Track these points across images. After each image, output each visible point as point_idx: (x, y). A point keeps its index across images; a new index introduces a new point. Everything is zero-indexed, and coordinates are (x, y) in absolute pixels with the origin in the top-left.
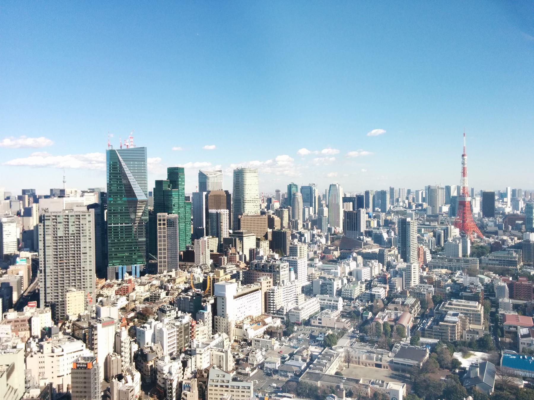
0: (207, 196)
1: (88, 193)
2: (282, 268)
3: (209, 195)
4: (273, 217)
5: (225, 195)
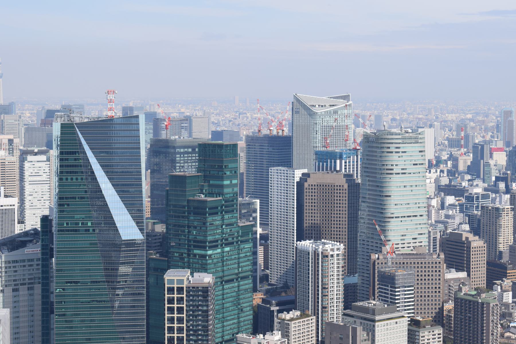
0: (300, 185)
1: (36, 154)
3: (306, 185)
4: (467, 238)
5: (346, 186)
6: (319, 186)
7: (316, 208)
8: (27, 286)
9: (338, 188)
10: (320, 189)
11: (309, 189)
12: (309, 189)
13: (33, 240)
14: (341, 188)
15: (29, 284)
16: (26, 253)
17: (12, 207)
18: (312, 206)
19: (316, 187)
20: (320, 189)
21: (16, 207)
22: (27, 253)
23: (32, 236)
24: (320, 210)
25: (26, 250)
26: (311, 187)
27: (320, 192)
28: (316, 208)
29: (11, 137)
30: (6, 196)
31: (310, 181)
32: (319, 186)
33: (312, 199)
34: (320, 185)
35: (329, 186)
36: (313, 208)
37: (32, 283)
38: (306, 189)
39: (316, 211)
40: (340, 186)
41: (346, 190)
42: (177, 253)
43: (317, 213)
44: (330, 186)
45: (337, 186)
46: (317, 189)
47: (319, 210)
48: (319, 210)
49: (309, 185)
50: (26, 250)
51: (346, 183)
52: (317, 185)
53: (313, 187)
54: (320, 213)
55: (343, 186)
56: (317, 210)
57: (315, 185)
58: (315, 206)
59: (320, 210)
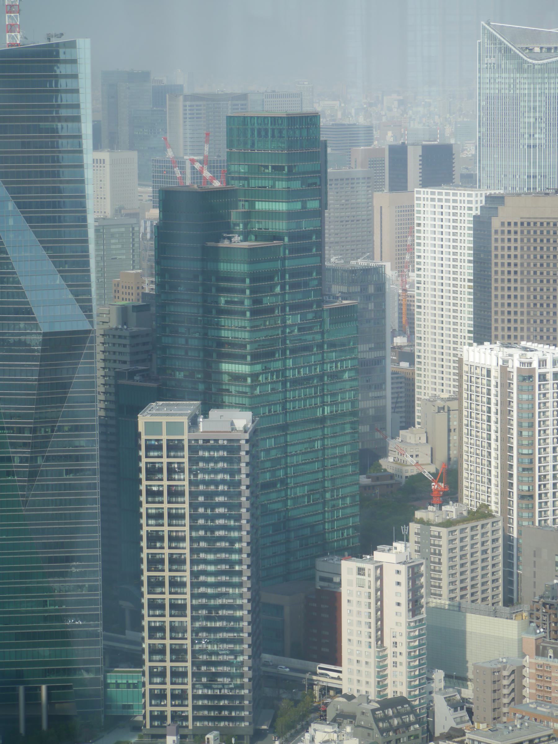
2: (361, 571)
6: (525, 224)
7: (519, 277)
10: (529, 232)
11: (503, 232)
18: (509, 264)
19: (519, 228)
20: (529, 232)
24: (529, 281)
26: (506, 229)
27: (529, 240)
28: (519, 277)
32: (525, 224)
33: (509, 232)
34: (529, 224)
36: (512, 277)
38: (496, 232)
39: (519, 285)
43: (522, 289)
46: (522, 232)
47: (525, 281)
48: (525, 281)
49: (503, 224)
52: (522, 224)
53: (512, 229)
54: (529, 289)
56: (522, 281)
57: (516, 224)
59: (529, 281)
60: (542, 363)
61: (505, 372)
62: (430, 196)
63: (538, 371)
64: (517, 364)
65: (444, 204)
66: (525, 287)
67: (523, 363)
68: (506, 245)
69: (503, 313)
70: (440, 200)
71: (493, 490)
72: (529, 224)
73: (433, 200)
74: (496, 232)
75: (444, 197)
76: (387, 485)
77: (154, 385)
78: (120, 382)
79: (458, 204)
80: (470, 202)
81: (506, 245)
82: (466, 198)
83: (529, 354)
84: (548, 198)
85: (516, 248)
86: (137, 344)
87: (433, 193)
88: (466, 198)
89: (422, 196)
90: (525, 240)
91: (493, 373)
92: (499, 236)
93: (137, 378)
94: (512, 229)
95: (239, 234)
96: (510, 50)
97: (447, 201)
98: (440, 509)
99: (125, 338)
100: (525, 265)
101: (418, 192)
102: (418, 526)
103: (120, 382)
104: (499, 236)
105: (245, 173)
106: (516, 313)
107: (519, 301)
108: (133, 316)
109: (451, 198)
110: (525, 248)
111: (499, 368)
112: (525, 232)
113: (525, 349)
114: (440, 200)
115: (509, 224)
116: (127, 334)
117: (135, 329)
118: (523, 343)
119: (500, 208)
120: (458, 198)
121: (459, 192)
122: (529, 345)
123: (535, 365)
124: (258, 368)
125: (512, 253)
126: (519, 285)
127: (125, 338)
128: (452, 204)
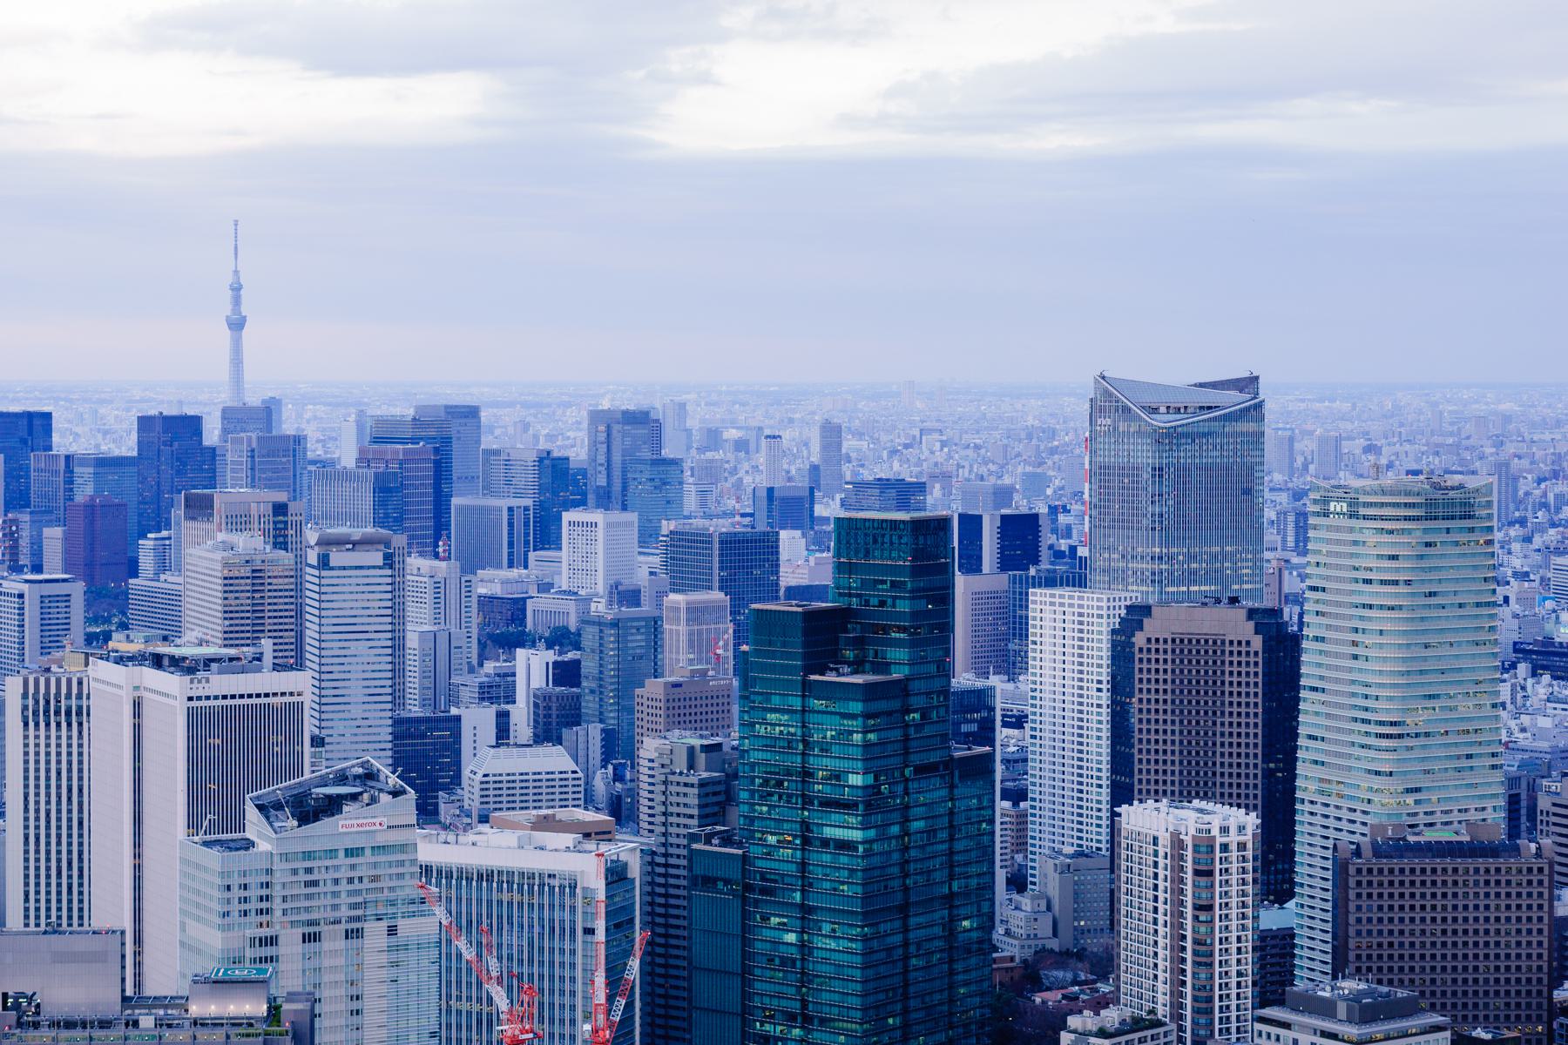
3: (1139, 639)
5: (1257, 643)
6: (1178, 641)
8: (343, 926)
9: (1235, 648)
11: (1149, 650)
12: (1149, 650)
13: (361, 793)
14: (1243, 649)
15: (351, 919)
16: (341, 830)
17: (295, 699)
21: (308, 700)
22: (345, 830)
23: (358, 782)
24: (1182, 712)
25: (341, 823)
26: (1153, 646)
29: (282, 497)
30: (276, 667)
31: (1153, 628)
32: (1178, 641)
35: (1206, 641)
37: (358, 919)
38: (1141, 650)
40: (1240, 643)
41: (1256, 654)
42: (772, 834)
44: (1211, 642)
45: (1231, 643)
47: (1177, 712)
48: (1177, 712)
49: (1149, 640)
50: (341, 823)
51: (1257, 633)
52: (1174, 641)
54: (1181, 722)
55: (1248, 643)
56: (1173, 712)
57: (1165, 641)
58: (1165, 681)
59: (1182, 712)
60: (1225, 830)
61: (1177, 843)
62: (1048, 599)
63: (1219, 840)
64: (1192, 831)
65: (1066, 609)
66: (1177, 719)
67: (1200, 831)
68: (1153, 666)
69: (1148, 751)
70: (1062, 605)
71: (1160, 987)
72: (1182, 641)
73: (1052, 604)
74: (1141, 650)
75: (1067, 601)
76: (1007, 969)
77: (740, 852)
78: (695, 846)
79: (1085, 611)
80: (1099, 608)
81: (1153, 666)
82: (1095, 603)
83: (1207, 818)
84: (1205, 610)
85: (1165, 671)
86: (707, 795)
87: (1053, 596)
88: (1095, 603)
89: (1038, 598)
90: (1178, 661)
91: (1160, 842)
92: (1145, 656)
93: (715, 841)
94: (1161, 646)
95: (849, 664)
96: (1130, 410)
97: (1071, 605)
98: (1098, 1014)
99: (692, 786)
100: (1177, 692)
101: (1035, 594)
102: (1073, 1036)
103: (695, 846)
104: (1145, 656)
105: (856, 588)
106: (1165, 742)
107: (1169, 737)
108: (701, 758)
109: (1076, 602)
110: (1177, 671)
111: (1168, 835)
112: (1178, 651)
113: (1201, 811)
114: (1062, 605)
115: (1157, 640)
116: (694, 780)
117: (705, 775)
118: (1196, 803)
119: (1146, 621)
120: (1085, 603)
121: (1086, 595)
122: (1203, 804)
123: (1215, 832)
124: (872, 833)
125: (1161, 676)
126: (1169, 717)
127: (692, 786)
128: (1076, 610)
